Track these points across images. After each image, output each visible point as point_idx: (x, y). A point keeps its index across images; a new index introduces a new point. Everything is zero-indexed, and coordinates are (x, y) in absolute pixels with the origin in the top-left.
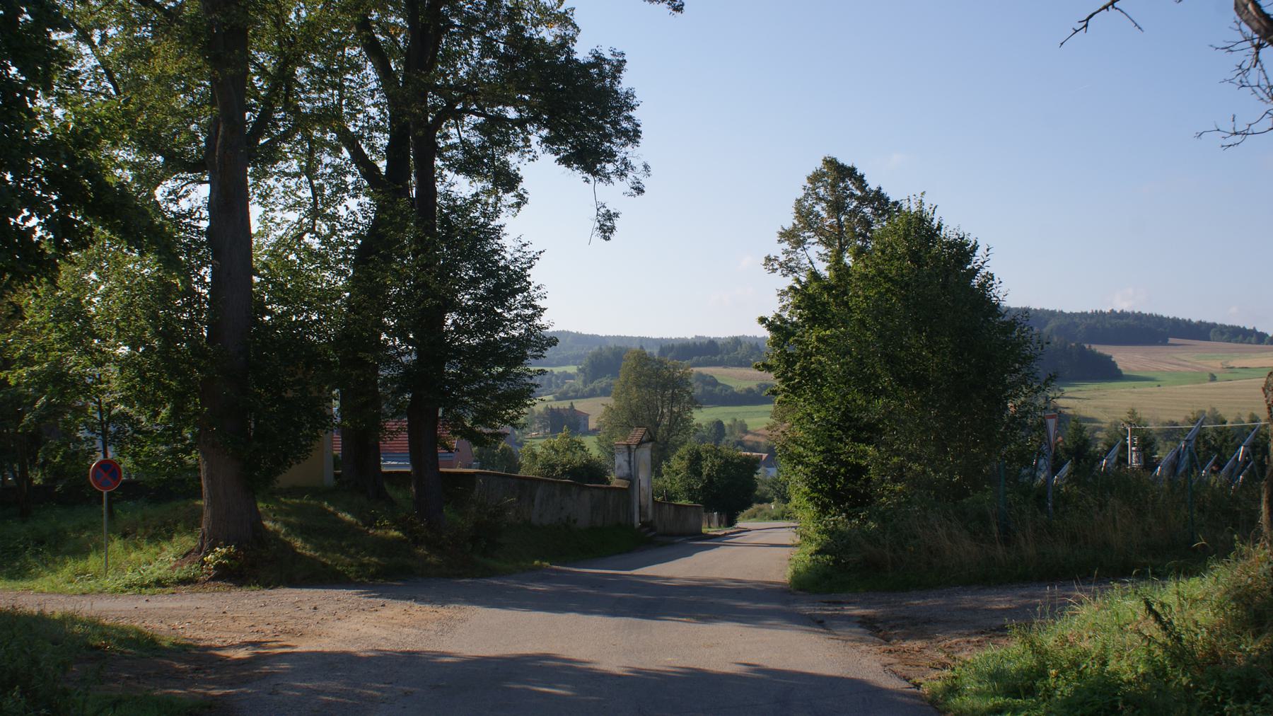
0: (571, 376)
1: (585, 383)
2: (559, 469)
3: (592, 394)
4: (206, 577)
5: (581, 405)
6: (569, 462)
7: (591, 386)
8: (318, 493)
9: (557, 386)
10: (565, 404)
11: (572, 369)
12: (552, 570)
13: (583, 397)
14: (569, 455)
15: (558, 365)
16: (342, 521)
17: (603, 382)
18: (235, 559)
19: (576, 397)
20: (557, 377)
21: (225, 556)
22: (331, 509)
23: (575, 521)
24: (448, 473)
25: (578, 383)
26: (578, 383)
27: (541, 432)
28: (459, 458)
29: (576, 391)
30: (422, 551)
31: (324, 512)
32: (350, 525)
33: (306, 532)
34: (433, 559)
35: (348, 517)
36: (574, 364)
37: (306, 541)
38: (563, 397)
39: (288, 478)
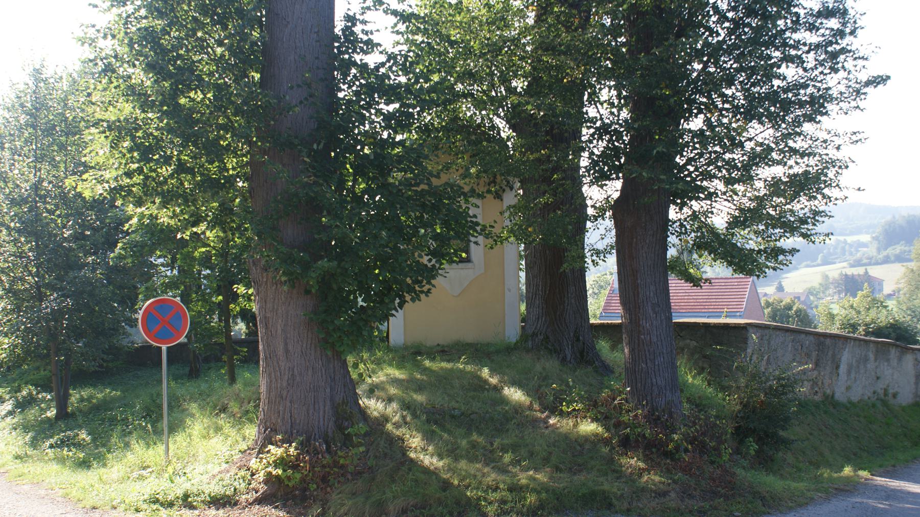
0: (865, 245)
1: (879, 250)
2: (861, 329)
3: (886, 261)
4: (252, 496)
5: (875, 272)
6: (873, 322)
7: (885, 253)
8: (480, 352)
9: (851, 254)
10: (860, 271)
11: (865, 238)
12: (877, 489)
13: (877, 263)
14: (873, 314)
15: (852, 233)
16: (504, 401)
17: (898, 249)
18: (295, 467)
19: (869, 264)
20: (851, 246)
21: (281, 462)
22: (494, 381)
23: (895, 396)
24: (706, 325)
25: (872, 251)
26: (872, 251)
27: (836, 297)
28: (709, 295)
29: (871, 259)
30: (632, 462)
31: (482, 385)
32: (518, 409)
33: (433, 421)
34: (654, 478)
35: (515, 395)
36: (867, 233)
37: (429, 437)
38: (858, 263)
39: (398, 327)
